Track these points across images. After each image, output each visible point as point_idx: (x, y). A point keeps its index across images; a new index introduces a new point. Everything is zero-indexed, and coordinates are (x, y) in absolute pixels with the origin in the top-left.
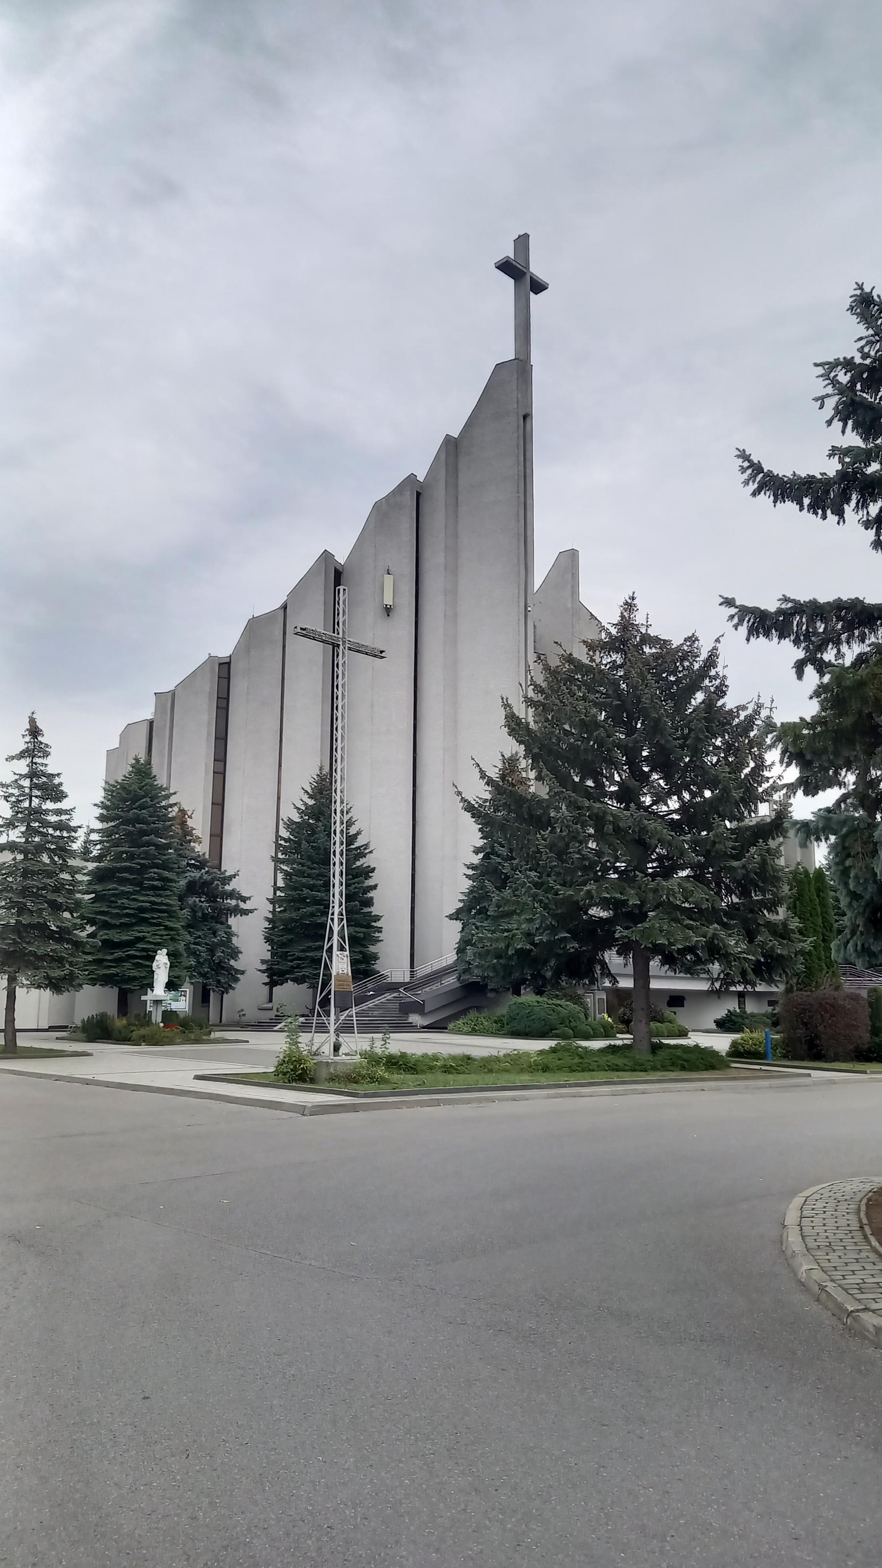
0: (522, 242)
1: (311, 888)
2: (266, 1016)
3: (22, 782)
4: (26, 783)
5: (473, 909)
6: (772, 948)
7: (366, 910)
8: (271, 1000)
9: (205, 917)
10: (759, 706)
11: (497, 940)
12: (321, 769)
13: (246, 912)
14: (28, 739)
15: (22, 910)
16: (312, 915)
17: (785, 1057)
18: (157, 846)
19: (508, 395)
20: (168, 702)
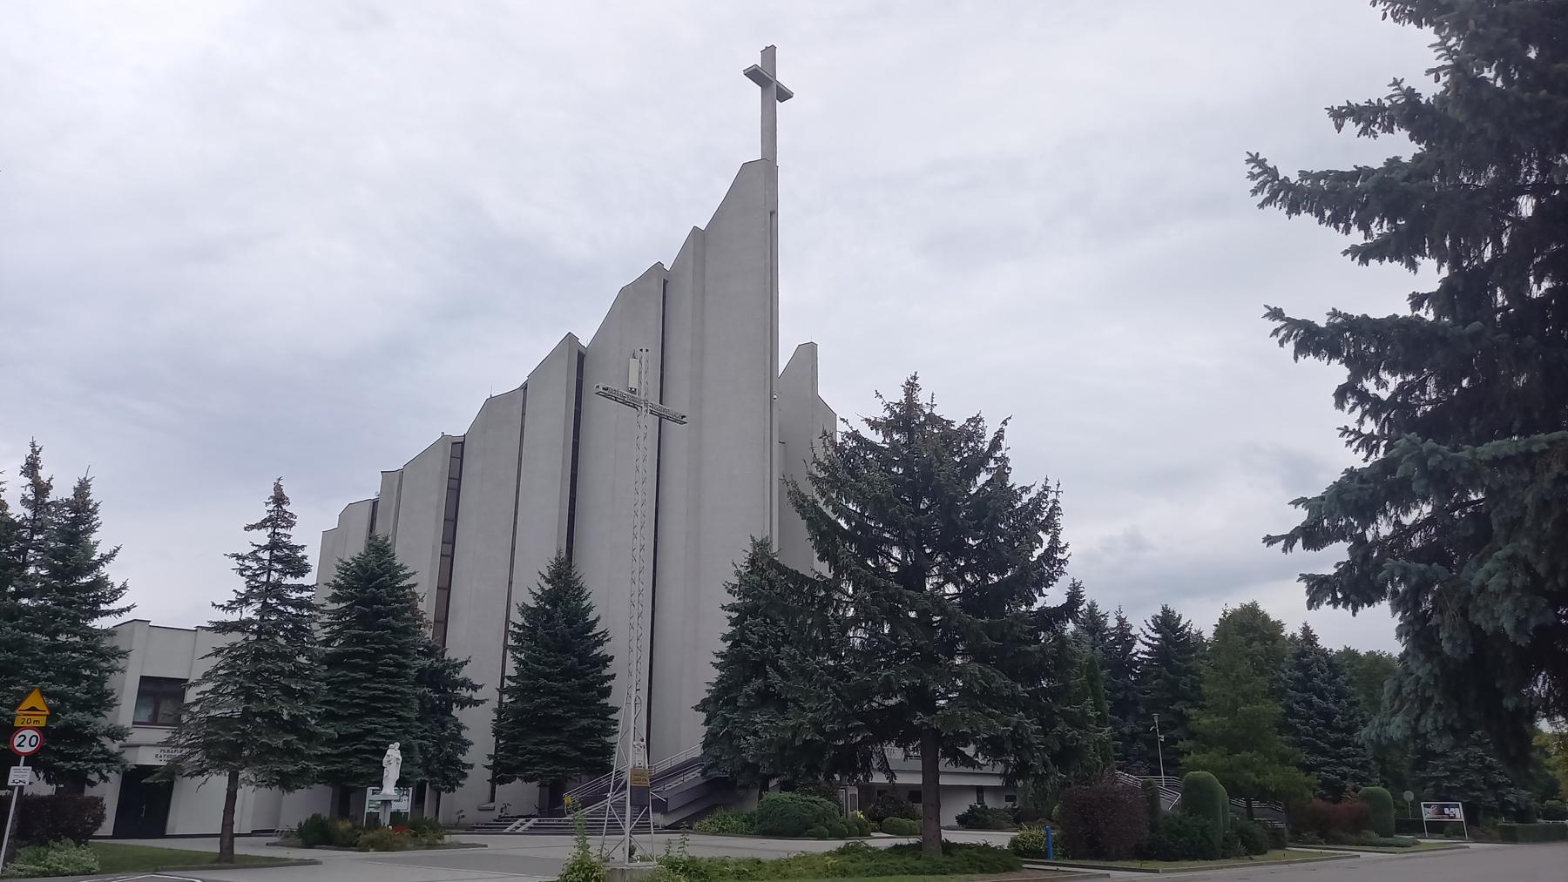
0: (769, 53)
1: (547, 677)
2: (490, 817)
3: (260, 554)
4: (266, 555)
5: (718, 703)
6: (1072, 739)
7: (604, 701)
8: (492, 800)
9: (434, 709)
10: (1046, 488)
11: (783, 729)
12: (559, 552)
13: (477, 703)
14: (271, 507)
15: (250, 696)
16: (547, 706)
17: (1064, 856)
18: (393, 629)
19: (756, 188)
20: (394, 481)
